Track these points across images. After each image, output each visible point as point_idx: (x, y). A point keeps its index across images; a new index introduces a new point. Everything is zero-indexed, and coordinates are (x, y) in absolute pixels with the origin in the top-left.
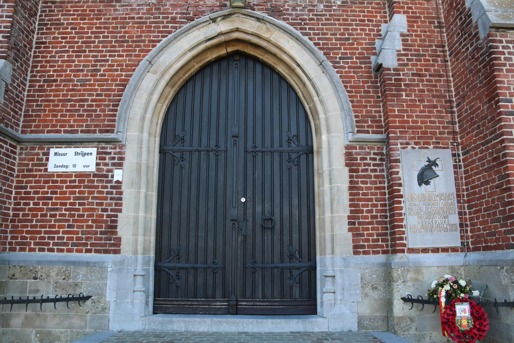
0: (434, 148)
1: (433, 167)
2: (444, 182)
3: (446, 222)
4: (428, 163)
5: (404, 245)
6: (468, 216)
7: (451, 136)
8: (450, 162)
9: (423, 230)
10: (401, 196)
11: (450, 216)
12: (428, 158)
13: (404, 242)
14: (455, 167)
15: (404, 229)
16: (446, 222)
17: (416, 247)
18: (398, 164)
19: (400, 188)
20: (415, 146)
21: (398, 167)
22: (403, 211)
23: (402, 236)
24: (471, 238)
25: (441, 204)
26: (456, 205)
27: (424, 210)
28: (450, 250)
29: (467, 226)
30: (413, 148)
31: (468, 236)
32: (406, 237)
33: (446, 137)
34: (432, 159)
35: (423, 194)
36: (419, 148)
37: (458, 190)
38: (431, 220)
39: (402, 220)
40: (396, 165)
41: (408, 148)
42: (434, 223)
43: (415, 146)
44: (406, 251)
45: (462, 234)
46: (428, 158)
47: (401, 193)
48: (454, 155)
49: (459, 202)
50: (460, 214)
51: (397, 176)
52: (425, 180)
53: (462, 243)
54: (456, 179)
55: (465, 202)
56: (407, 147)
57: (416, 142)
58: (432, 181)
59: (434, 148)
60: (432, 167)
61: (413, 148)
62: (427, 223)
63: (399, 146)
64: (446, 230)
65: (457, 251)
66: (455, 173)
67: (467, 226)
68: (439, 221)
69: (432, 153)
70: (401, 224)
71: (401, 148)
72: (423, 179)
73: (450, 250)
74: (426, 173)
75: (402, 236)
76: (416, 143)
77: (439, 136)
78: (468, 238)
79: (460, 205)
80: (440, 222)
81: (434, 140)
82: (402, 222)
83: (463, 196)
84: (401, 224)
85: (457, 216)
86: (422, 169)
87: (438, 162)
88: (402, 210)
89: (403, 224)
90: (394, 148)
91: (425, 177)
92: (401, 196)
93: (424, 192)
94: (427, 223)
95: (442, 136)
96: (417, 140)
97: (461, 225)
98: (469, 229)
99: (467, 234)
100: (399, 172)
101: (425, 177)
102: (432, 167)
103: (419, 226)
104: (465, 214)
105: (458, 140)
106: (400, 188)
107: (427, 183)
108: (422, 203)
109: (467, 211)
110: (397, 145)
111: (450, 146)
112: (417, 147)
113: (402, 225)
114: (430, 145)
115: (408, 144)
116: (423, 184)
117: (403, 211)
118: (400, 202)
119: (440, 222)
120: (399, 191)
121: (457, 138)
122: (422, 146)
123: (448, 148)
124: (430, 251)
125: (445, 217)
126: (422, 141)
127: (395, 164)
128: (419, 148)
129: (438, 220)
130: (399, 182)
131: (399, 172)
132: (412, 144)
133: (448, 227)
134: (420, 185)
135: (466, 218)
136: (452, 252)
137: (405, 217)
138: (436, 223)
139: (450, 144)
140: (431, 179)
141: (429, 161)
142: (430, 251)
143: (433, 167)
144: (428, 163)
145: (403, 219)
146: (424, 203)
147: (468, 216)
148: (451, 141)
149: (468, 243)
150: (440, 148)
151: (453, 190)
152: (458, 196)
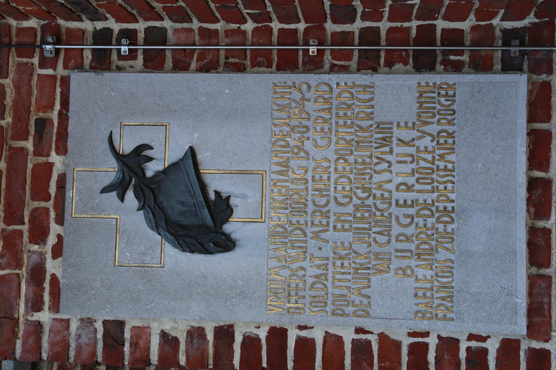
0: (62, 150)
1: (151, 169)
2: (231, 126)
3: (407, 135)
4: (130, 195)
5: (509, 347)
6: (384, 25)
7: (14, 60)
8: (133, 84)
9: (442, 255)
10: (278, 335)
11: (380, 116)
12: (105, 190)
13: (492, 346)
14: (154, 63)
15: (432, 342)
16: (407, 135)
17: (522, 302)
18: (127, 335)
19: (238, 339)
20: (52, 240)
21: (141, 333)
22: (348, 337)
23: (463, 354)
24: (493, 15)
25: (322, 151)
26: (333, 78)
27: (348, 237)
28: (538, 126)
29: (426, 35)
30: (57, 252)
31: (474, 28)
32: (471, 337)
33: (17, 87)
34: (110, 170)
35: (272, 234)
36: (60, 220)
37: (261, 61)
38: (395, 210)
39: (389, 346)
40: (134, 345)
41: (59, 275)
42: (410, 196)
43: (52, 240)
44: (537, 345)
45: (465, 58)
46: (105, 190)
47: (263, 334)
48: (102, 63)
49: (314, 65)
50: (369, 63)
51: (182, 347)
52: (209, 221)
53: (510, 66)
54: (209, 66)
55: (316, 32)
56: (54, 279)
57: (31, 230)
58: (216, 184)
59: (62, 150)
60: (149, 174)
61: (57, 252)
62: (410, 231)
63: (45, 316)
64: (447, 141)
65: (546, 88)
66: (181, 66)
67: (426, 35)
68: (401, 173)
69: (86, 169)
70: (405, 351)
71: (55, 307)
72: (203, 227)
73: (538, 126)
74: (174, 210)
75: (463, 354)
76: (39, 234)
77: (9, 119)
78: (484, 36)
79: (328, 58)
80: (407, 168)
81: (29, 145)
82: (398, 344)
83: (288, 37)
84: (405, 351)
85: (379, 80)
86: (156, 227)
87: (127, 146)
88: (339, 340)
89: (406, 342)
90: (52, 344)
91: (194, 218)
92: (278, 335)
93: (261, 230)
94: (410, 231)
95: (9, 101)
96: (25, 228)
97: (424, 63)
98: (441, 24)
99: (468, 39)
100: (164, 335)
101: (194, 218)
102: (149, 174)
103: (420, 272)
104: (370, 36)
105: (32, 30)
106: (238, 339)
107: (222, 208)
108: (312, 243)
109: (359, 24)
110: (39, 325)
111: (61, 71)
112: (55, 229)
113: (413, 347)
114: (50, 166)
115: (37, 273)
116: (228, 228)
117: (348, 337)
118: (305, 346)
119: (407, 168)
120: (251, 343)
121: (20, 31)
122: (50, 204)
123: (65, 82)
124: (541, 224)
125: (386, 141)
126: (31, 205)
127: (127, 349)
128: (60, 220)
129: (395, 175)
130: (210, 337)
131: (164, 335)
132: (42, 255)
133: (433, 129)
134: (227, 244)
135: (391, 30)
136: (548, 118)
137: (377, 331)
138: (409, 188)
139: (50, 72)
140: (203, 187)
141: (119, 188)
142: (541, 224)
143: (151, 169)
144: (130, 195)
145: (383, 337)
146: (316, 236)
147: (384, 25)
148: (36, 60)
149: (509, 36)
150: (64, 117)
151: (258, 85)
152: (287, 63)
